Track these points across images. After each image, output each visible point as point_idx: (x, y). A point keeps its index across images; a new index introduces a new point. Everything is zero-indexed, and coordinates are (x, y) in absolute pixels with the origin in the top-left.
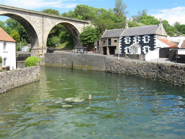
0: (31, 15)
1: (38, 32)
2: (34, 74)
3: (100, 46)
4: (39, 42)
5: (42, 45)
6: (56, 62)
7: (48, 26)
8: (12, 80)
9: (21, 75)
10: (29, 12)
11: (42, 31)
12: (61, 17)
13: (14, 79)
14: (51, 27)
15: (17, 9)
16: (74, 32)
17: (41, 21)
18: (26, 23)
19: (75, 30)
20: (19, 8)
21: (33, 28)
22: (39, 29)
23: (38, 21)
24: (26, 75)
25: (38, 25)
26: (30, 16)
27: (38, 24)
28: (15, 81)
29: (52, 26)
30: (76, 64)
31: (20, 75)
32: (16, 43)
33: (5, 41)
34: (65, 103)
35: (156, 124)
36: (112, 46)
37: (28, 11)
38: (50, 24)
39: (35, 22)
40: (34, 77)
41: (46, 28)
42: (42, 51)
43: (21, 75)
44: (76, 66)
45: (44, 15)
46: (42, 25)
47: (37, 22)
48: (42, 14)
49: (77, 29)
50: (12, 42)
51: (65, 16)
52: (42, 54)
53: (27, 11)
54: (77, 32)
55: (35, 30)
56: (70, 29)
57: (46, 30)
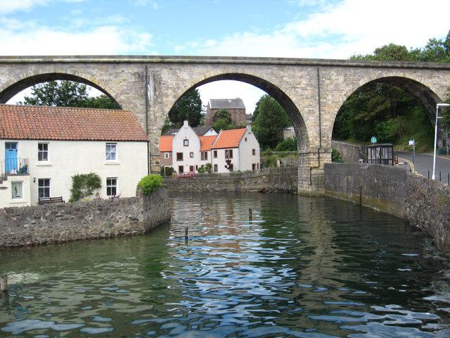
0: (283, 70)
1: (307, 110)
4: (310, 136)
5: (317, 143)
9: (62, 216)
10: (278, 62)
12: (374, 65)
13: (33, 224)
14: (344, 93)
15: (244, 61)
17: (314, 82)
19: (428, 93)
20: (251, 58)
22: (307, 102)
25: (306, 93)
26: (282, 73)
27: (303, 89)
28: (36, 229)
29: (348, 90)
31: (58, 217)
34: (344, 284)
35: (142, 318)
38: (340, 89)
39: (298, 89)
41: (330, 97)
42: (319, 158)
43: (62, 216)
45: (321, 65)
46: (317, 90)
47: (302, 86)
51: (353, 62)
52: (317, 165)
53: (273, 62)
55: (296, 105)
56: (417, 94)
57: (330, 102)
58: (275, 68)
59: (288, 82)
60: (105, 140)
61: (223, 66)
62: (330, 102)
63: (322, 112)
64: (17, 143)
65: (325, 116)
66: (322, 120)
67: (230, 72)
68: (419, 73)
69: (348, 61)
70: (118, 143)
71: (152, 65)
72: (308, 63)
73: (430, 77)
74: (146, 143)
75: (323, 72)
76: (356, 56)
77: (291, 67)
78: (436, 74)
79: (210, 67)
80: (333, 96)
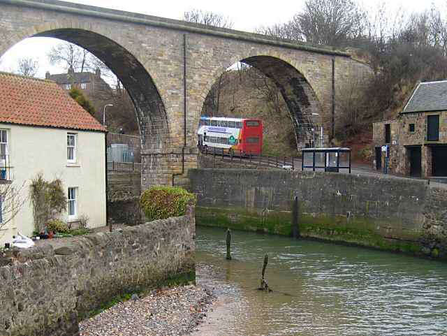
1: (169, 92)
2: (178, 244)
3: (394, 142)
6: (236, 203)
7: (204, 72)
8: (111, 263)
10: (137, 19)
11: (183, 89)
13: (117, 260)
16: (294, 91)
17: (179, 54)
18: (126, 63)
21: (151, 79)
22: (171, 82)
23: (167, 52)
24: (152, 248)
30: (311, 210)
32: (106, 133)
33: (73, 129)
36: (441, 141)
37: (133, 18)
40: (176, 256)
41: (196, 77)
44: (309, 214)
45: (190, 31)
48: (392, 132)
49: (307, 78)
50: (94, 131)
52: (180, 171)
54: (306, 89)
55: (157, 85)
57: (196, 84)
58: (131, 28)
59: (142, 47)
60: (67, 129)
61: (64, 16)
62: (196, 84)
63: (188, 98)
64: (438, 116)
65: (191, 104)
66: (187, 109)
67: (74, 27)
68: (295, 54)
69: (265, 36)
70: (80, 133)
71: (193, 35)
72: (245, 37)
73: (305, 61)
74: (103, 135)
75: (191, 40)
76: (386, 41)
77: (151, 29)
78: (310, 57)
79: (44, 16)
80: (200, 76)
